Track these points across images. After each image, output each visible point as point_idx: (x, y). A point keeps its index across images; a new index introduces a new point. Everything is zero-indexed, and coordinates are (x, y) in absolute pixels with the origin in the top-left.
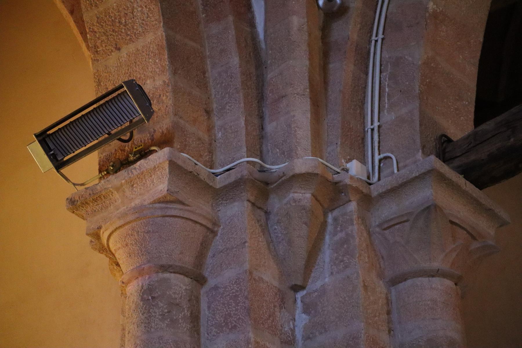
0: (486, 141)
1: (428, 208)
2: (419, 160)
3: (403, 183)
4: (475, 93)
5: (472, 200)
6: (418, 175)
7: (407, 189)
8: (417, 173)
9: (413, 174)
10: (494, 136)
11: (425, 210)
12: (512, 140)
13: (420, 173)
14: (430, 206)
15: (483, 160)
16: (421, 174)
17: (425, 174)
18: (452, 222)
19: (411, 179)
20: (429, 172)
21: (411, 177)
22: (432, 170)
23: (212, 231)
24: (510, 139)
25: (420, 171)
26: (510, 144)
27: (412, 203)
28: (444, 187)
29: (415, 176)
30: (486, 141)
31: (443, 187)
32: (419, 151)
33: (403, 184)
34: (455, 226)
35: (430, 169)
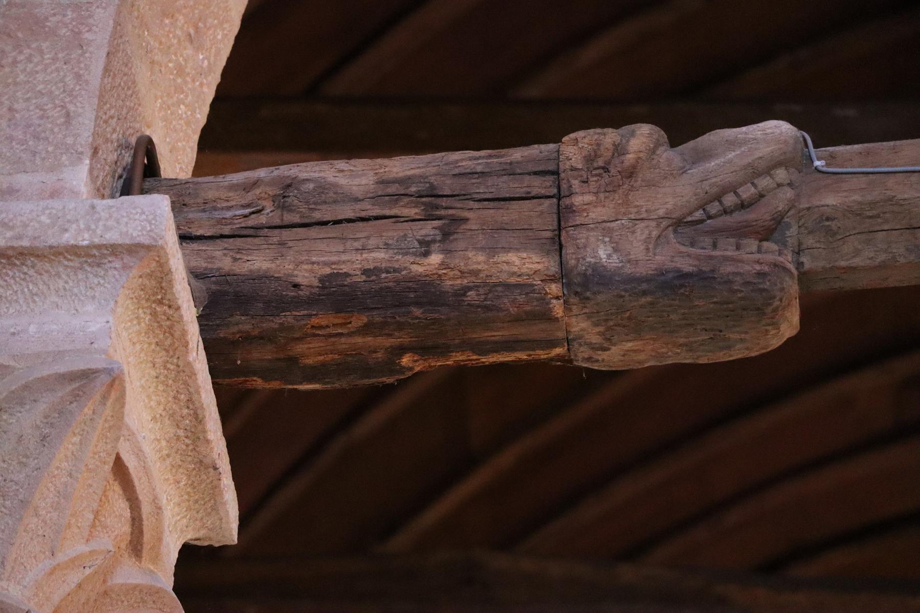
0: (325, 223)
1: (86, 376)
2: (75, 193)
3: (13, 248)
4: (232, 42)
5: (185, 411)
6: (85, 243)
7: (13, 277)
8: (86, 236)
9: (67, 235)
10: (362, 219)
11: (72, 377)
12: (435, 259)
13: (97, 241)
14: (96, 371)
15: (296, 286)
16: (99, 247)
17: (114, 250)
18: (120, 468)
19: (51, 247)
20: (134, 249)
21: (52, 241)
22: (148, 248)
23: (326, 202)
24: (426, 254)
25: (99, 232)
26: (420, 269)
27: (13, 334)
28: (143, 325)
29: (72, 242)
30: (325, 223)
31: (139, 324)
32: (80, 160)
33: (10, 253)
34: (117, 488)
35: (145, 241)
